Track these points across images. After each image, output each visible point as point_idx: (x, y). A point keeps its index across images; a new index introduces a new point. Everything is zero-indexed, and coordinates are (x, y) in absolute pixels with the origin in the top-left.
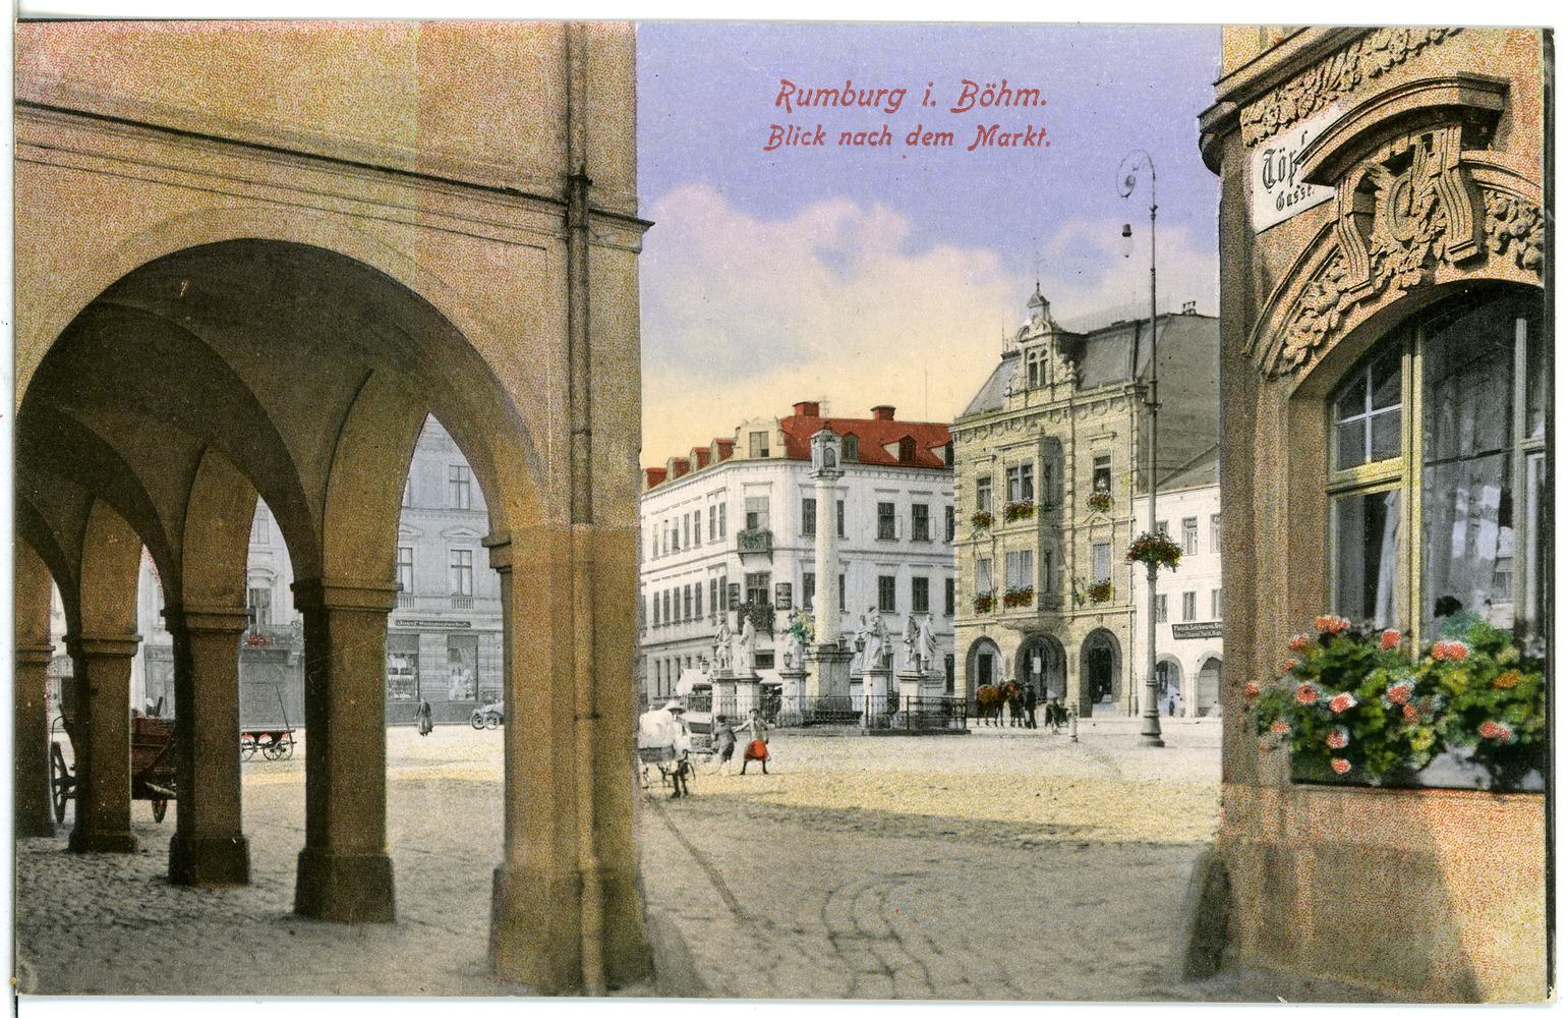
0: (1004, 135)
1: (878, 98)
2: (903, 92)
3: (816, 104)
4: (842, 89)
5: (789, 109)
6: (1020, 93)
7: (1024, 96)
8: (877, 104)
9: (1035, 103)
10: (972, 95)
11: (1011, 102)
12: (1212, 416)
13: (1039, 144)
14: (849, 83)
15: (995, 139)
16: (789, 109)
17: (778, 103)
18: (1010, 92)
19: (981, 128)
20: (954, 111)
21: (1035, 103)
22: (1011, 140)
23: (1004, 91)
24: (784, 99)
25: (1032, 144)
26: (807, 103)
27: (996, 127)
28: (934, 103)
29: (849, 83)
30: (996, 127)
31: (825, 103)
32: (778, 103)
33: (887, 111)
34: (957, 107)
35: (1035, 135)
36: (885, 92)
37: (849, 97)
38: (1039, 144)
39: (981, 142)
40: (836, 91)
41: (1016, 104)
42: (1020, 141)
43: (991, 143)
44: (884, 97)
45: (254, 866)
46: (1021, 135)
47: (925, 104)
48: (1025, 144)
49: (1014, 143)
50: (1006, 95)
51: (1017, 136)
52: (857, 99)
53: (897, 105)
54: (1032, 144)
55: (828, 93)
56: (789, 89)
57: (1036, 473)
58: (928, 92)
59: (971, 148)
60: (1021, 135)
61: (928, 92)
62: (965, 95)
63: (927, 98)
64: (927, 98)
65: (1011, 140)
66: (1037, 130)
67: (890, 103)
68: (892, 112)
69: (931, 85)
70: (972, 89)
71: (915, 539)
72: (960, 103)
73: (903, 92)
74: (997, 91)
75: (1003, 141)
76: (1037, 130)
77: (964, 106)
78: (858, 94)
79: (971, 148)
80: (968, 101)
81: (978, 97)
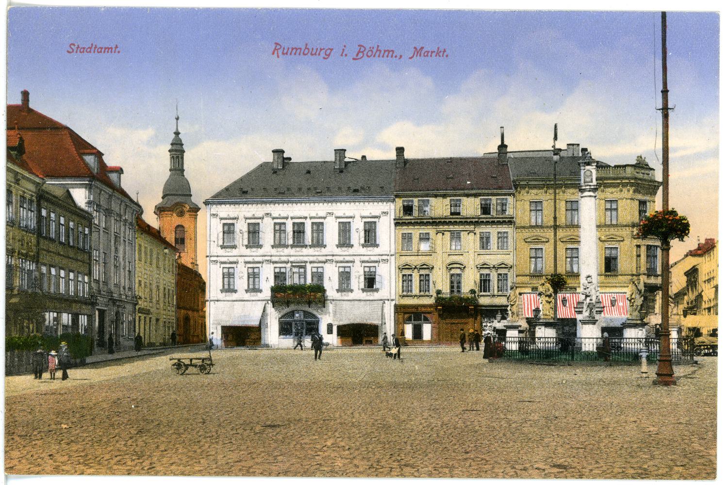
0: (427, 51)
1: (320, 52)
2: (332, 50)
3: (291, 54)
4: (303, 48)
5: (278, 57)
6: (385, 51)
7: (387, 53)
8: (319, 54)
9: (392, 56)
10: (363, 52)
11: (381, 55)
12: (114, 295)
13: (443, 56)
14: (306, 45)
15: (422, 55)
16: (278, 57)
17: (273, 53)
18: (380, 51)
19: (415, 48)
20: (354, 59)
21: (392, 56)
22: (430, 54)
23: (377, 50)
24: (276, 52)
25: (440, 56)
26: (287, 53)
27: (422, 48)
28: (346, 55)
29: (306, 45)
30: (422, 48)
31: (295, 54)
32: (273, 53)
33: (324, 58)
34: (355, 57)
35: (440, 52)
36: (324, 49)
37: (306, 51)
38: (443, 56)
39: (415, 55)
40: (301, 49)
41: (383, 56)
42: (434, 54)
43: (420, 56)
44: (323, 51)
45: (619, 267)
46: (434, 52)
47: (342, 55)
48: (436, 56)
49: (431, 56)
50: (378, 52)
51: (432, 52)
52: (310, 52)
53: (329, 55)
54: (440, 56)
55: (297, 49)
56: (278, 47)
57: (451, 198)
58: (343, 50)
59: (411, 58)
60: (434, 52)
61: (343, 50)
62: (359, 52)
63: (343, 53)
64: (343, 53)
65: (430, 54)
66: (441, 49)
67: (326, 55)
68: (327, 58)
69: (345, 46)
70: (362, 49)
71: (340, 245)
72: (357, 55)
73: (332, 50)
74: (374, 50)
75: (426, 55)
76: (441, 49)
77: (358, 57)
78: (311, 50)
79: (411, 58)
80: (361, 55)
81: (365, 53)
